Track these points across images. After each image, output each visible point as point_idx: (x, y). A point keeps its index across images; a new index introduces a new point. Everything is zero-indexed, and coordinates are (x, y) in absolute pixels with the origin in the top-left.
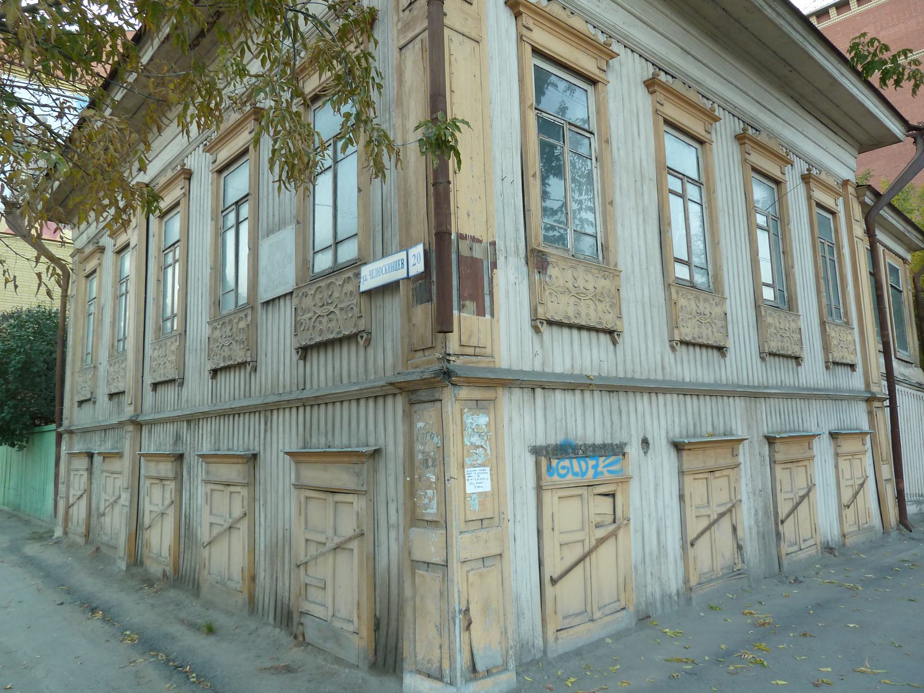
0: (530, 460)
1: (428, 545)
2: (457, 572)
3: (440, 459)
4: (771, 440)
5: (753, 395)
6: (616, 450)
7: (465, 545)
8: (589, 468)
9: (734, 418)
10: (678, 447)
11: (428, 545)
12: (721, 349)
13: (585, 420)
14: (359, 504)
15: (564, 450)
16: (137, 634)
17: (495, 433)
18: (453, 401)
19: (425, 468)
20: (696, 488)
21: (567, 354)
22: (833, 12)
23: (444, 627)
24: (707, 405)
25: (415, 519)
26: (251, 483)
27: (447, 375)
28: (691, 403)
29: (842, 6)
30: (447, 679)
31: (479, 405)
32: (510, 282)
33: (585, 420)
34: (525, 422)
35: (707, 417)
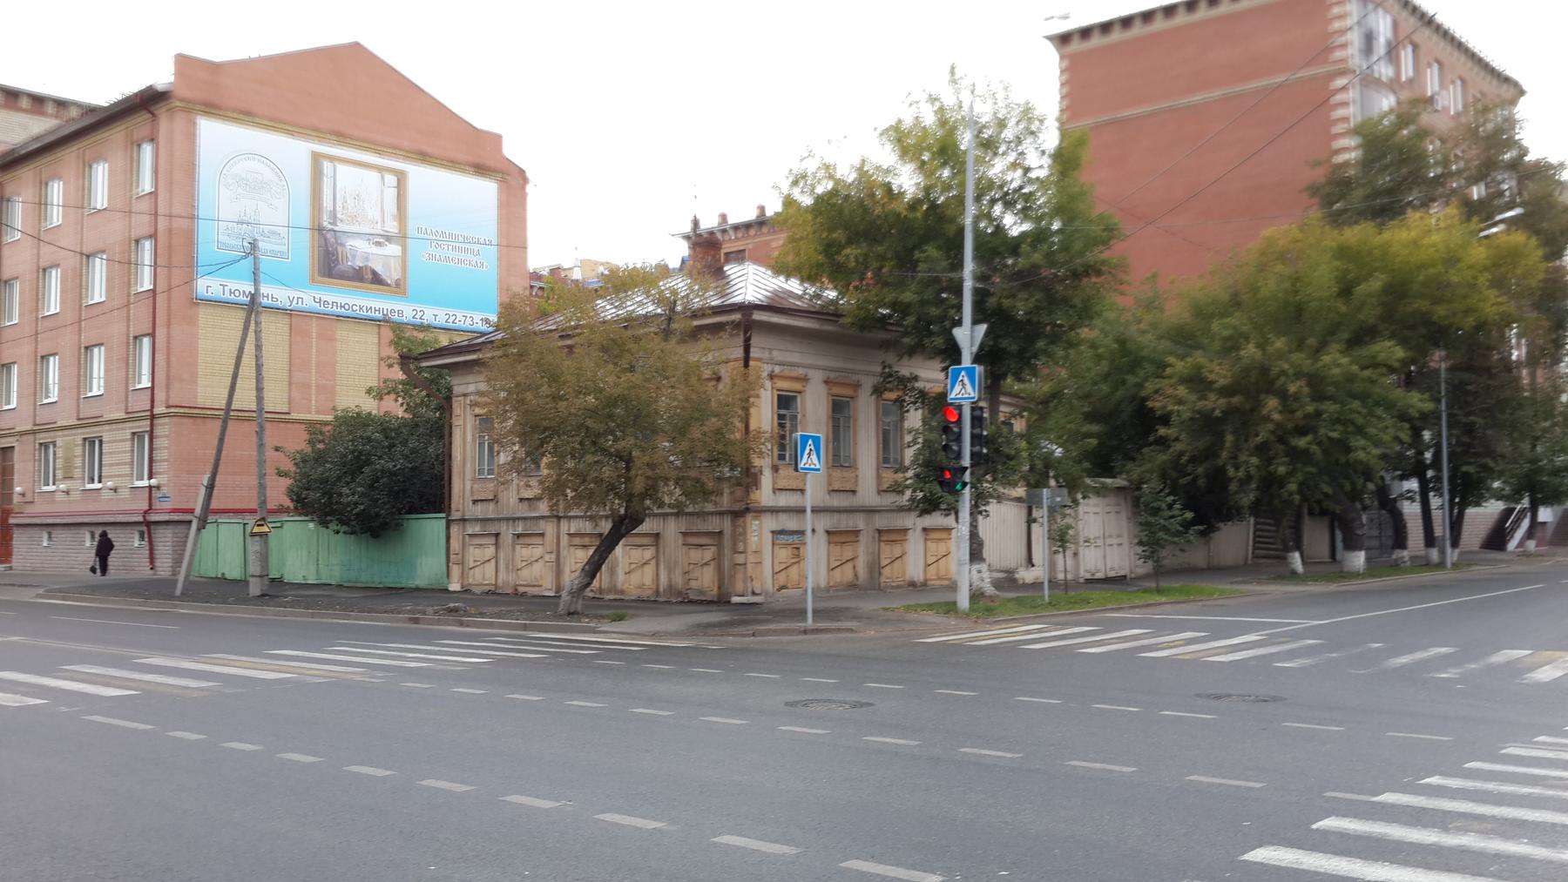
0: (770, 536)
1: (740, 559)
2: (749, 566)
3: (744, 534)
4: (880, 531)
5: (870, 511)
6: (802, 533)
7: (752, 558)
8: (791, 539)
9: (859, 522)
10: (828, 532)
11: (740, 559)
12: (854, 492)
13: (790, 523)
14: (713, 549)
15: (782, 532)
16: (1437, 177)
17: (760, 526)
18: (749, 517)
19: (739, 536)
20: (837, 550)
21: (784, 500)
22: (1182, 11)
23: (745, 581)
24: (844, 516)
25: (736, 552)
26: (657, 545)
27: (747, 510)
28: (836, 516)
29: (1191, 6)
30: (797, 386)
31: (755, 518)
32: (766, 480)
33: (790, 523)
34: (770, 523)
35: (846, 522)
